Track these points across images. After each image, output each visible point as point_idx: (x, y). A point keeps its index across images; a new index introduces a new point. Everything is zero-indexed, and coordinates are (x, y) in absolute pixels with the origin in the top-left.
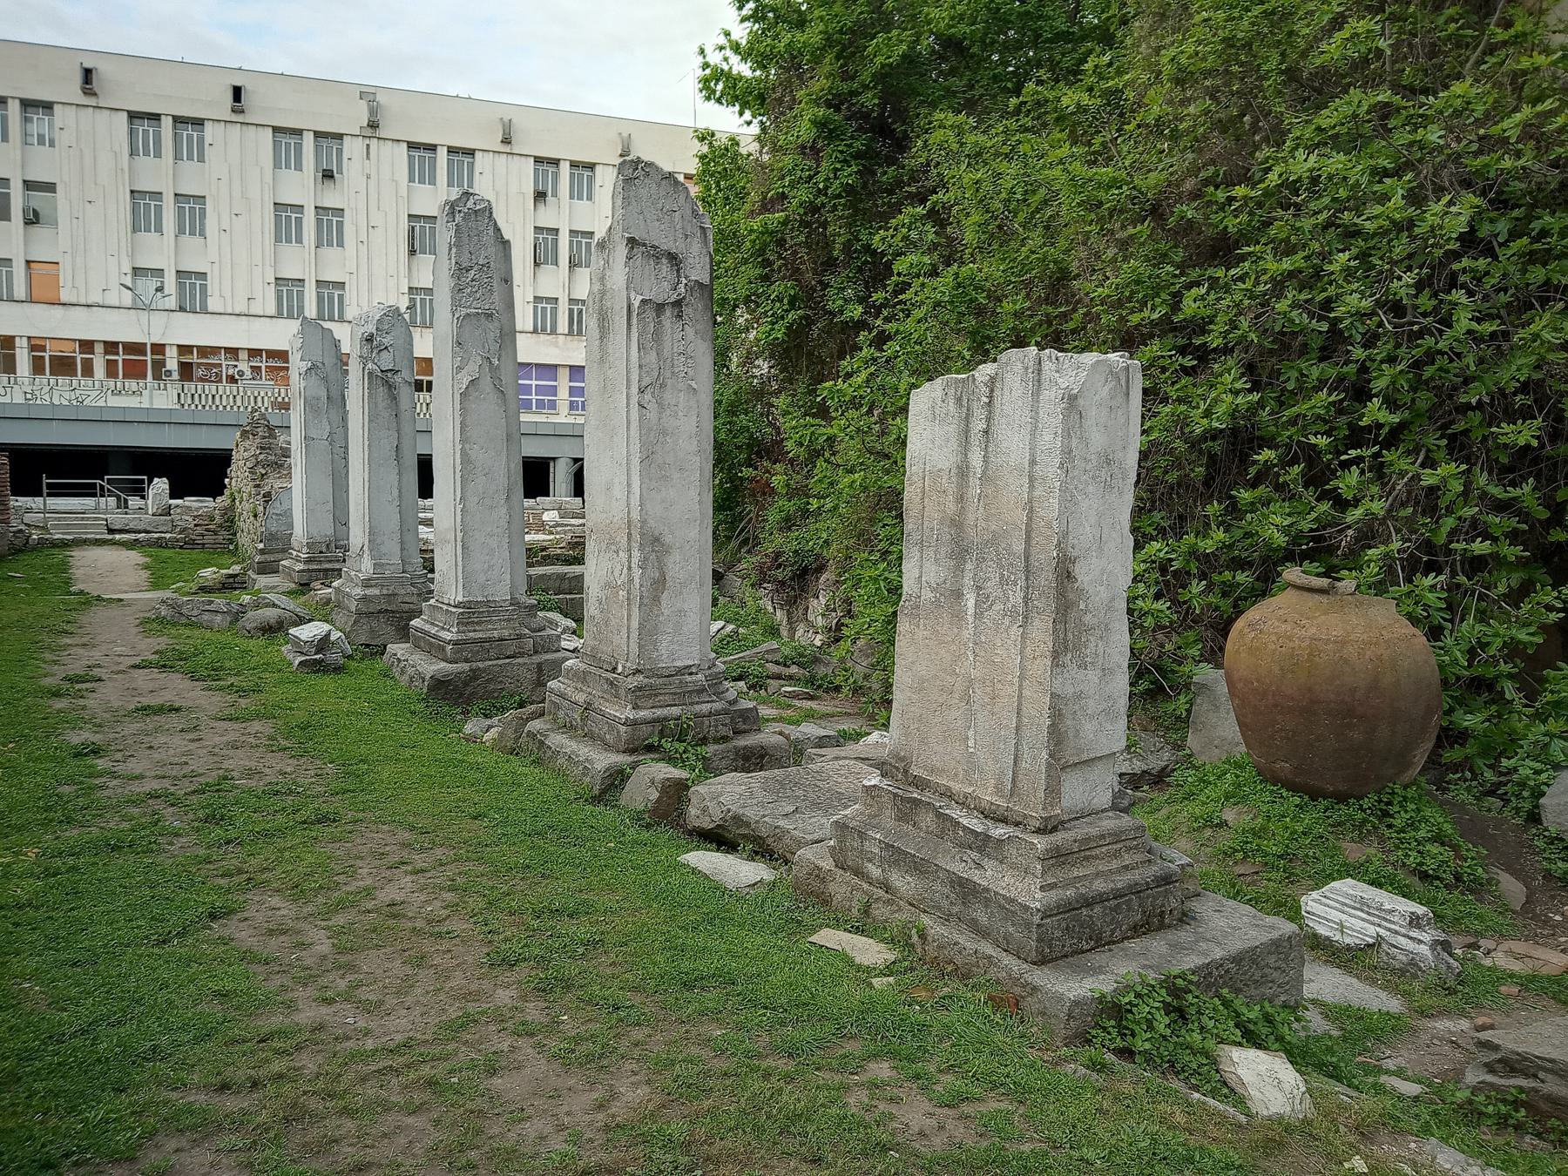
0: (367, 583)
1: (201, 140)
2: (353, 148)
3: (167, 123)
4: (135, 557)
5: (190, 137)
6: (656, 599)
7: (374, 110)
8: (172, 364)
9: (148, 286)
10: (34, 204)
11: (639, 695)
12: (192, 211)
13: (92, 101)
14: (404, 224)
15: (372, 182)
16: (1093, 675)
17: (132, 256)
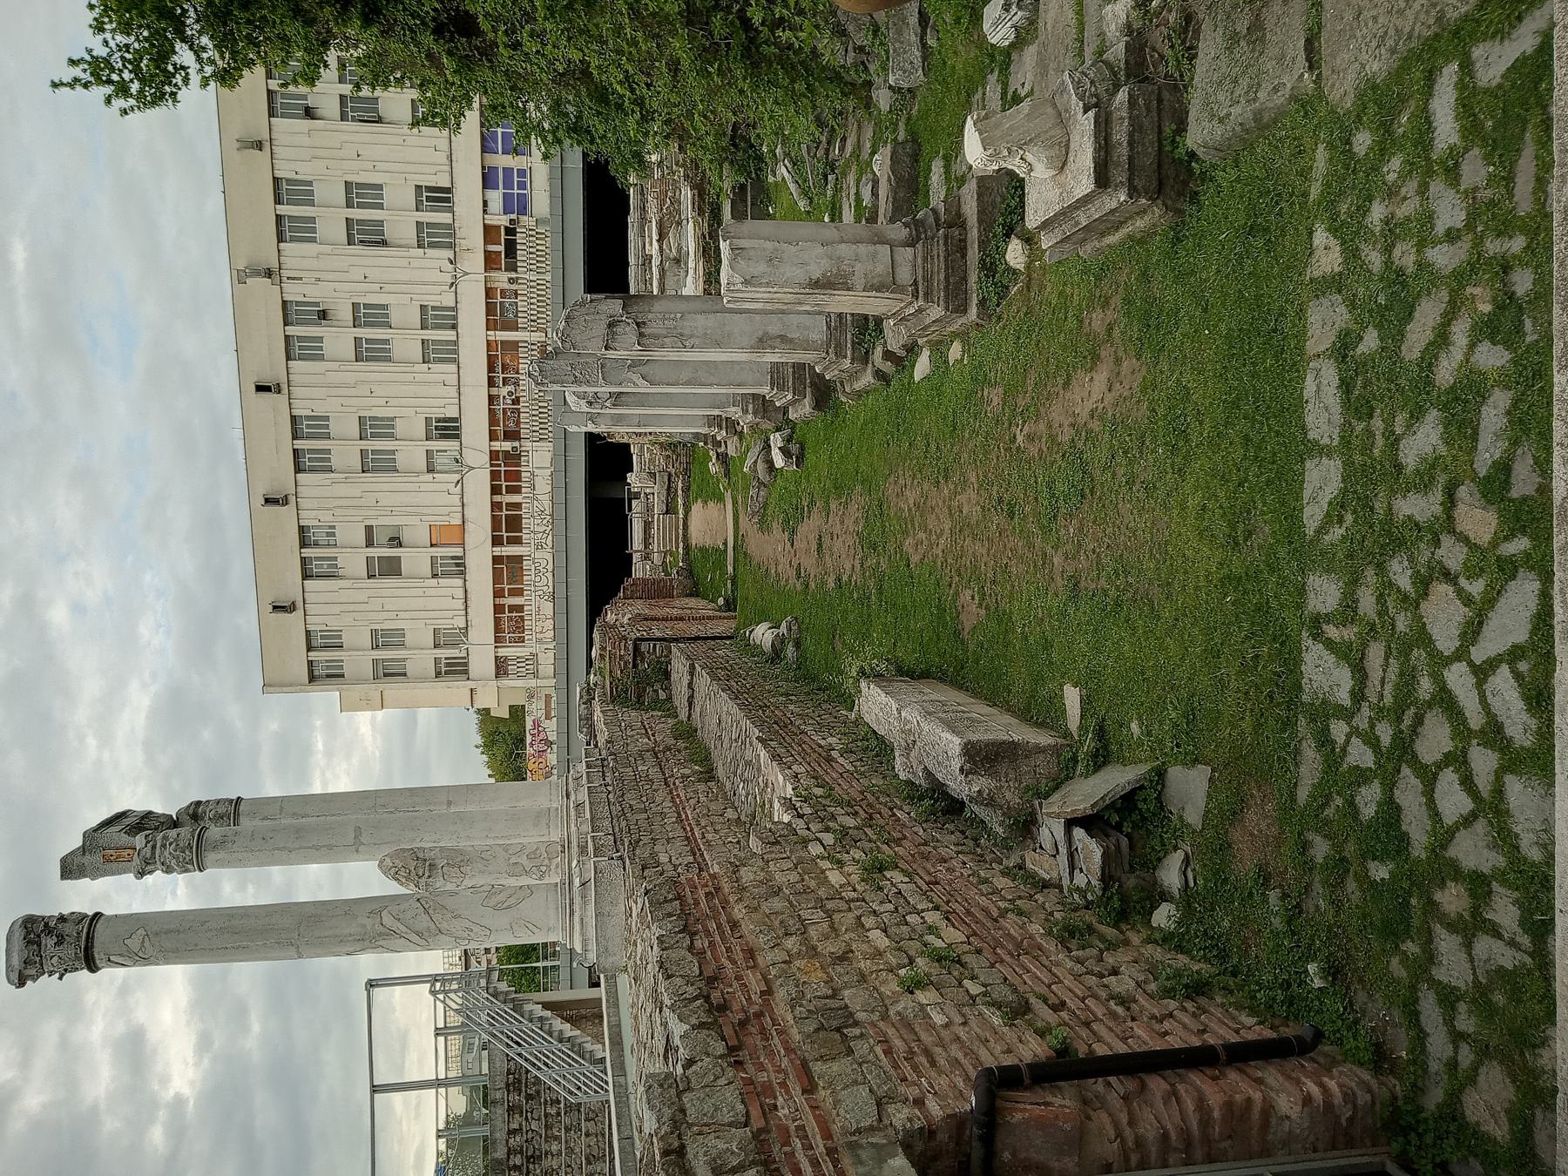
0: (745, 412)
1: (308, 418)
2: (294, 292)
3: (299, 444)
4: (697, 508)
5: (308, 426)
6: (791, 341)
7: (256, 273)
8: (507, 446)
9: (440, 461)
10: (384, 540)
11: (840, 354)
12: (372, 427)
13: (292, 499)
14: (357, 249)
15: (322, 276)
16: (858, 267)
17: (419, 473)
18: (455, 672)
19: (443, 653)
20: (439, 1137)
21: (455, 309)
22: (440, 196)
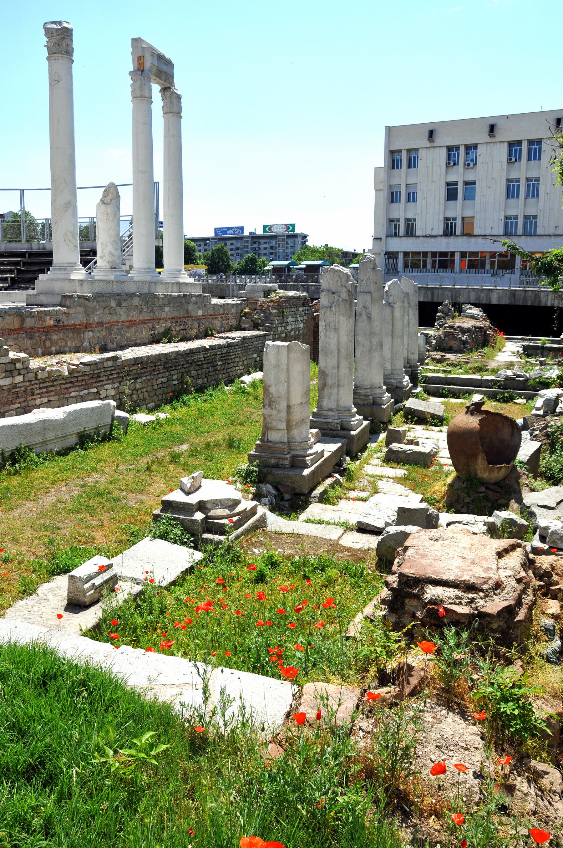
1: (540, 149)
5: (516, 150)
16: (274, 412)
18: (447, 228)
19: (459, 222)
20: (46, 220)
21: (535, 235)
22: (410, 232)
